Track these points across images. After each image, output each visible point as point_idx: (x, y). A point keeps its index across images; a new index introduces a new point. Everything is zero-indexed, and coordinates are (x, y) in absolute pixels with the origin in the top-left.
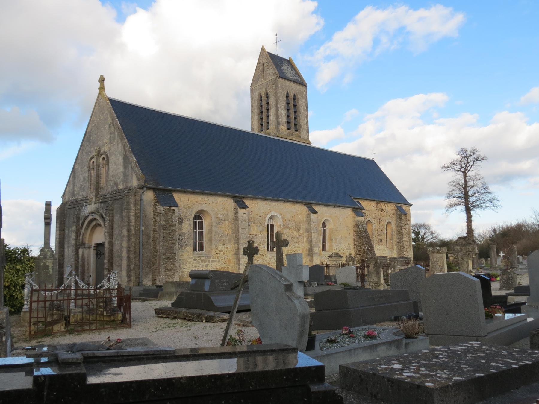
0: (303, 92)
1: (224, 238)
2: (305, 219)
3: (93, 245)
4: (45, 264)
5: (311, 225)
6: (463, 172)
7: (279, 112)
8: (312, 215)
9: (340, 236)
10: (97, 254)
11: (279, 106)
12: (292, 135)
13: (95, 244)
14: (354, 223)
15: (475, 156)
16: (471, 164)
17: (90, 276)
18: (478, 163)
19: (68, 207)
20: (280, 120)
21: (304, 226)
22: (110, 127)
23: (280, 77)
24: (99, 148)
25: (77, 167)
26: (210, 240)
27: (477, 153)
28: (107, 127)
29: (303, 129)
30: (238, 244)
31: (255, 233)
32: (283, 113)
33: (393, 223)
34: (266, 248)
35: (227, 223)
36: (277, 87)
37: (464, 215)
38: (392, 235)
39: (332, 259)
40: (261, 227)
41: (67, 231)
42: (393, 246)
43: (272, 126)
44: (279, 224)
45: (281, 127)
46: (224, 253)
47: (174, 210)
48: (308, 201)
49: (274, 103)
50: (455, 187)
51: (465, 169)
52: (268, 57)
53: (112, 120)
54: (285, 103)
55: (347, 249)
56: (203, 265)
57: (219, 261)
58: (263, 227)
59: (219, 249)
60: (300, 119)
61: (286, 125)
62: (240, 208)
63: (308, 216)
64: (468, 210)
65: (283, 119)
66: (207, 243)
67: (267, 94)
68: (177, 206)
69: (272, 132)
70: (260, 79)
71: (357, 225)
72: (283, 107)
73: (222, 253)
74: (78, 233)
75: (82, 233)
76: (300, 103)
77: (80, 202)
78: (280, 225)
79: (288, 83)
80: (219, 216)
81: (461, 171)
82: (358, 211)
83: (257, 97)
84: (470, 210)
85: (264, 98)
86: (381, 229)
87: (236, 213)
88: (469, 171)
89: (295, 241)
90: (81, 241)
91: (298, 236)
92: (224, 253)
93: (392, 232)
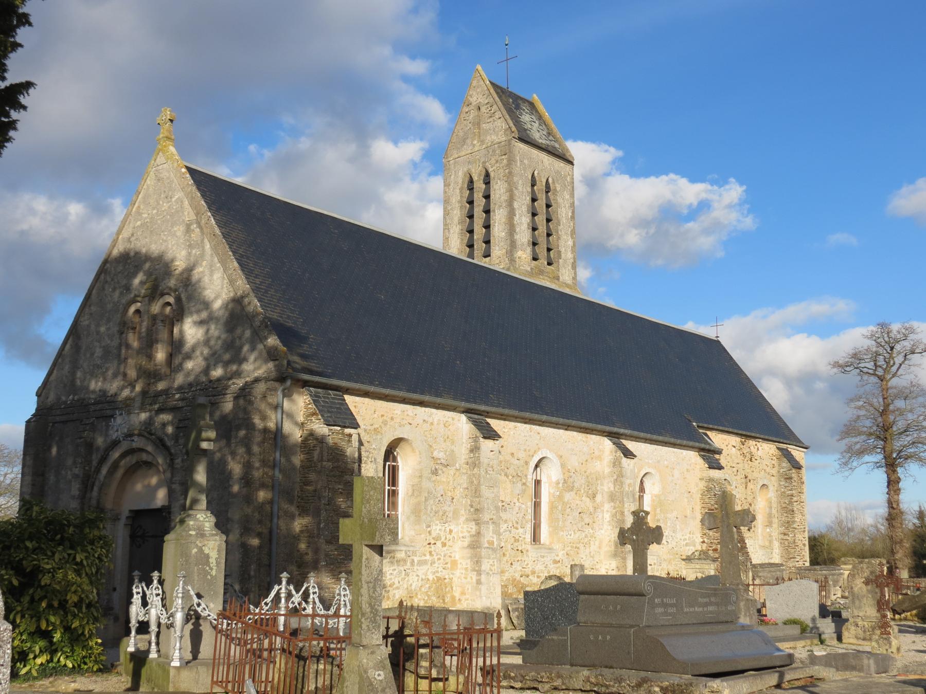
0: (566, 176)
1: (446, 508)
2: (607, 470)
3: (125, 513)
4: (201, 550)
5: (622, 483)
6: (879, 377)
7: (516, 218)
8: (624, 459)
9: (675, 514)
10: (133, 537)
11: (516, 205)
12: (541, 272)
13: (131, 511)
14: (702, 485)
15: (907, 344)
16: (899, 359)
17: (115, 589)
18: (915, 358)
19: (58, 419)
20: (517, 237)
21: (607, 486)
22: (188, 230)
23: (521, 139)
24: (156, 279)
25: (85, 322)
26: (416, 512)
27: (912, 336)
28: (180, 230)
29: (565, 261)
30: (477, 524)
31: (507, 500)
32: (523, 221)
33: (771, 488)
34: (528, 537)
35: (451, 471)
36: (511, 161)
37: (881, 476)
38: (770, 516)
39: (693, 566)
40: (519, 485)
41: (52, 478)
42: (771, 542)
43: (498, 249)
44: (554, 479)
45: (520, 253)
46: (444, 545)
47: (350, 435)
48: (615, 430)
49: (505, 197)
50: (862, 413)
51: (885, 370)
52: (492, 91)
53: (197, 214)
54: (529, 198)
55: (687, 545)
56: (400, 572)
57: (433, 563)
58: (524, 484)
59: (434, 534)
60: (559, 238)
61: (529, 250)
62: (485, 438)
63: (616, 463)
64: (891, 465)
65: (523, 235)
66: (408, 518)
67: (487, 175)
68: (356, 426)
69: (497, 261)
70: (469, 141)
71: (709, 490)
72: (525, 209)
73: (439, 544)
74: (87, 482)
75: (97, 483)
76: (560, 200)
77: (93, 408)
78: (558, 483)
79: (535, 152)
80: (435, 454)
81: (874, 374)
82: (711, 456)
83: (460, 181)
84: (897, 466)
85: (480, 186)
86: (749, 500)
87: (475, 449)
88: (894, 376)
89: (587, 521)
90: (94, 502)
91: (592, 510)
92: (444, 545)
93: (771, 508)
